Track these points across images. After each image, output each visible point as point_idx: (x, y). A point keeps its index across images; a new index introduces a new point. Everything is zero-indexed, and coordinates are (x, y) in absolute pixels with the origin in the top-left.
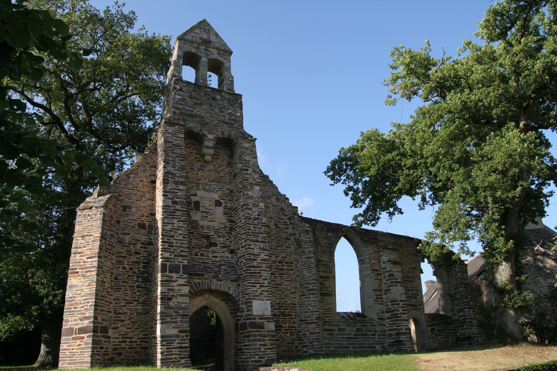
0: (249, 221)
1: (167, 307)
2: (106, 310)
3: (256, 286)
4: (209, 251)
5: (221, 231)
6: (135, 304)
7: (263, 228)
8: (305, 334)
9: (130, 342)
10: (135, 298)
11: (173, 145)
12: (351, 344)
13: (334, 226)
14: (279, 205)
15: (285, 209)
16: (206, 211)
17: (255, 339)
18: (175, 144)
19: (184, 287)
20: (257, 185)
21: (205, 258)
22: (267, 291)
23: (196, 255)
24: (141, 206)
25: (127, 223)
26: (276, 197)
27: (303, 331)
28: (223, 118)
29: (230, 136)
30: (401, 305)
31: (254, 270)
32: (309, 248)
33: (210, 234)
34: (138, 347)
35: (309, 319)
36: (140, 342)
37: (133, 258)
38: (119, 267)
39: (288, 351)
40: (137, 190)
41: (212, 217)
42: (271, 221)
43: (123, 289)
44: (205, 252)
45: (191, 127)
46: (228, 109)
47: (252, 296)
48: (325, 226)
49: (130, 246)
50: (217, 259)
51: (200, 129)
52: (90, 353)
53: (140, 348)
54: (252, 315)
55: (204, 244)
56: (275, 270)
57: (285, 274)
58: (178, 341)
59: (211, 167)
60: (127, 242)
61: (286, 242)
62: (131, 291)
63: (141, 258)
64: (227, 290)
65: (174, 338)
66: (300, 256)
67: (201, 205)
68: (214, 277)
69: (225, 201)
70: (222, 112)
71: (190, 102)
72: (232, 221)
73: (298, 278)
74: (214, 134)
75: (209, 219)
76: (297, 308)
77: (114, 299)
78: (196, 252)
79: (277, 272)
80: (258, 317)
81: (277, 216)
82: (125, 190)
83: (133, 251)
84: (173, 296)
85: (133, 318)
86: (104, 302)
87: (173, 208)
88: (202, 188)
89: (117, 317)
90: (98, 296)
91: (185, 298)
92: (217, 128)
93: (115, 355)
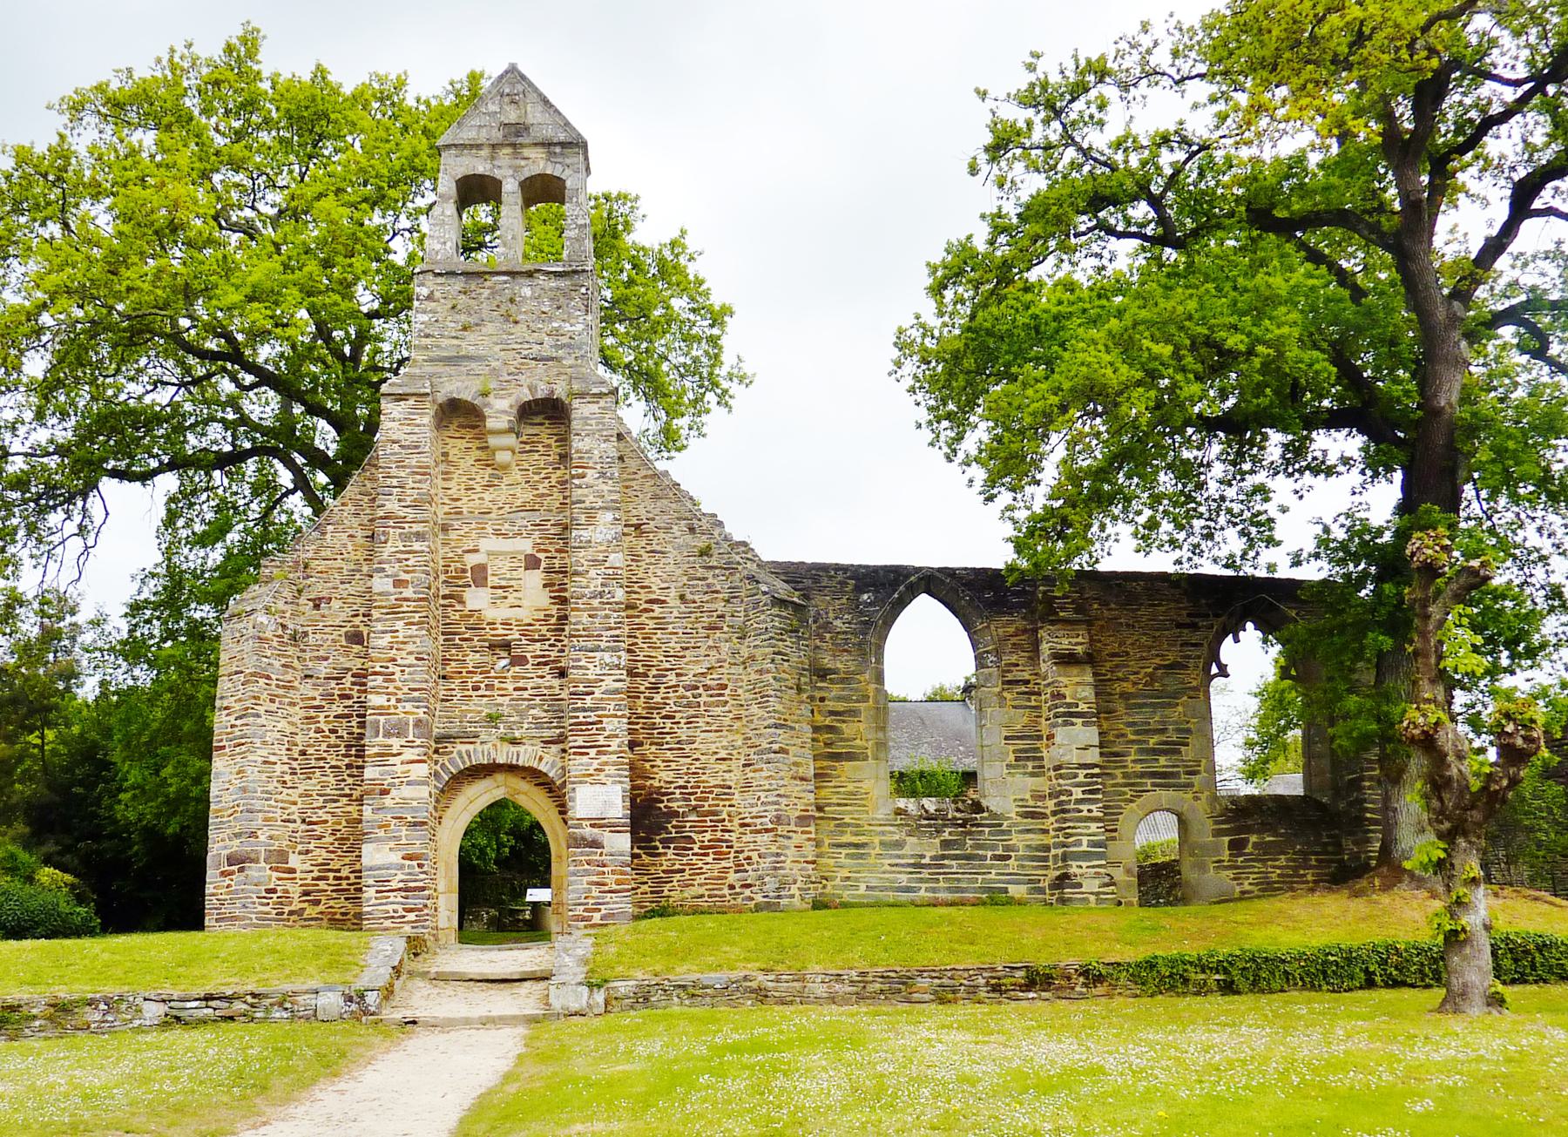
7: (615, 614)
8: (749, 858)
9: (336, 878)
12: (921, 880)
13: (881, 572)
16: (503, 583)
18: (407, 443)
20: (606, 508)
22: (615, 764)
23: (476, 689)
30: (1081, 779)
35: (758, 821)
38: (309, 729)
43: (318, 774)
46: (551, 319)
48: (849, 578)
57: (704, 716)
60: (322, 676)
67: (490, 572)
72: (564, 601)
76: (736, 797)
80: (588, 823)
84: (393, 785)
86: (272, 803)
92: (520, 377)
93: (305, 905)
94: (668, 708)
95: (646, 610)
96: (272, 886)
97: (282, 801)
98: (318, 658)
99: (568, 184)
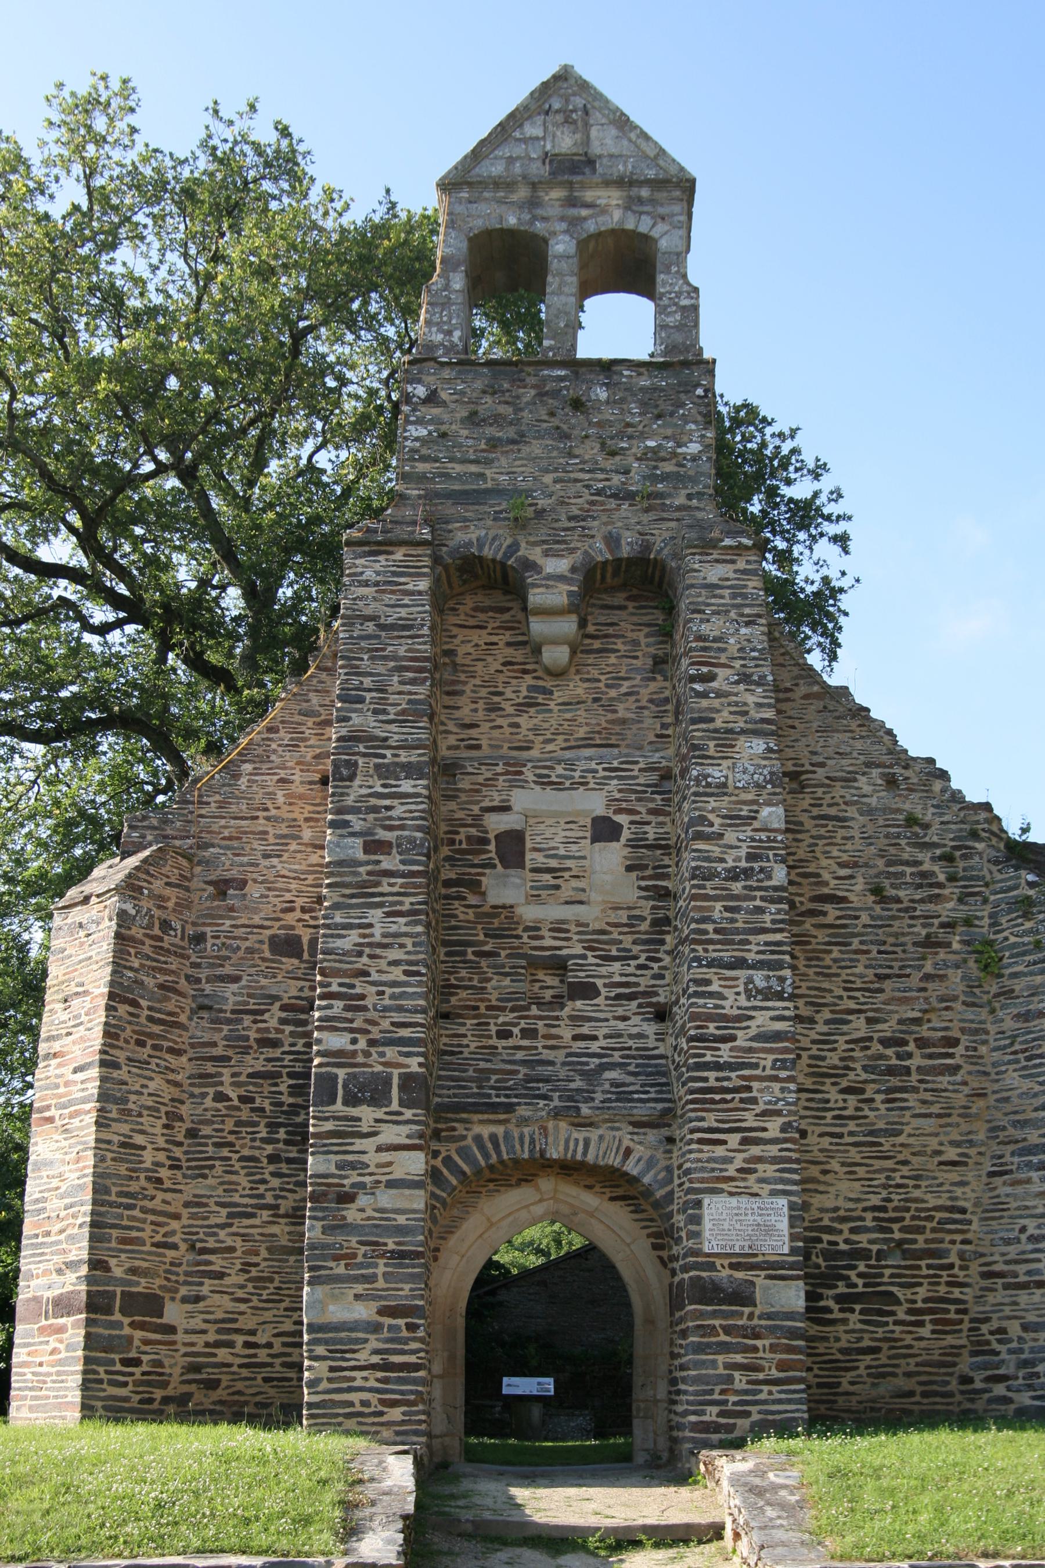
0: (704, 887)
1: (334, 1228)
2: (148, 1242)
3: (724, 1142)
4: (557, 1018)
5: (615, 936)
6: (265, 1218)
7: (773, 908)
8: (1002, 1331)
9: (247, 1345)
10: (261, 1196)
11: (382, 627)
14: (897, 803)
15: (928, 818)
16: (553, 863)
17: (709, 1345)
18: (390, 620)
19: (405, 1153)
20: (756, 733)
21: (540, 1043)
22: (774, 1160)
23: (504, 1034)
24: (285, 872)
25: (229, 942)
26: (883, 775)
27: (994, 1316)
28: (617, 479)
29: (647, 547)
31: (717, 1079)
32: (1032, 974)
33: (564, 952)
34: (278, 1361)
35: (1022, 1268)
36: (285, 1345)
37: (252, 1063)
38: (204, 1095)
39: (925, 1394)
40: (268, 819)
41: (581, 884)
42: (851, 877)
43: (219, 1170)
44: (541, 1023)
45: (470, 543)
46: (643, 436)
47: (702, 1180)
49: (239, 1021)
50: (595, 1047)
51: (509, 541)
52: (79, 1378)
53: (284, 1365)
54: (697, 1253)
55: (548, 994)
56: (864, 1076)
57: (915, 1090)
58: (374, 1344)
59: (577, 688)
60: (229, 1007)
61: (924, 959)
62: (248, 1175)
63: (282, 1060)
64: (614, 1160)
65: (361, 1335)
66: (993, 1011)
67: (529, 845)
68: (556, 1114)
69: (637, 818)
70: (613, 454)
71: (470, 442)
72: (664, 894)
73: (981, 1103)
74: (572, 551)
75: (566, 893)
76: (974, 1226)
77: (187, 1205)
78: (504, 1024)
79: (874, 1081)
80: (726, 1262)
81: (882, 853)
82: (223, 822)
83: (253, 1035)
84: (362, 1186)
85: (257, 1265)
86: (136, 1213)
87: (369, 868)
88: (532, 778)
89: (199, 1264)
90: (108, 1192)
91: (407, 1192)
92: (590, 523)
93: (193, 1388)
94: (852, 1075)
95: (812, 913)
96: (133, 1354)
97: (154, 1212)
98: (222, 979)
99: (663, 244)
